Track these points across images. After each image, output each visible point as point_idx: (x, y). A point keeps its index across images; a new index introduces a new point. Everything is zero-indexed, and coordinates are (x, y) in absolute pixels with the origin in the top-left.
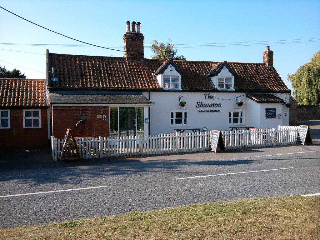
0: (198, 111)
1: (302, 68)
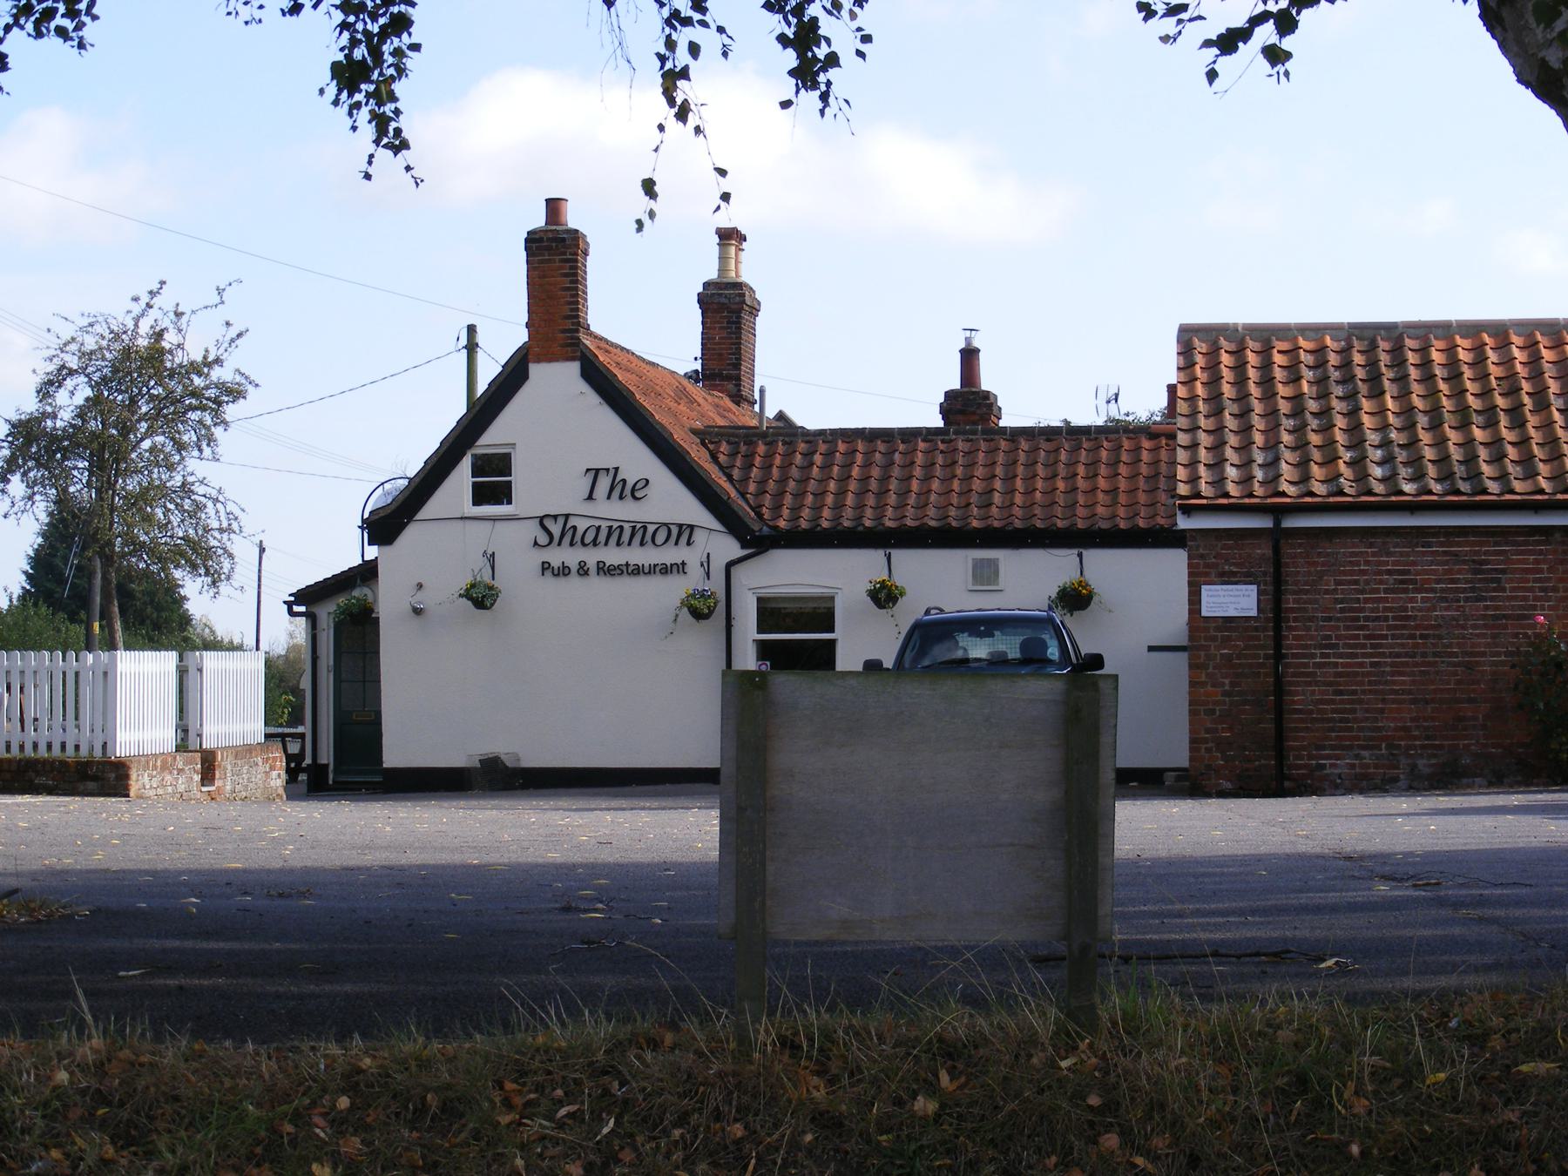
0: (543, 569)
1: (759, 303)
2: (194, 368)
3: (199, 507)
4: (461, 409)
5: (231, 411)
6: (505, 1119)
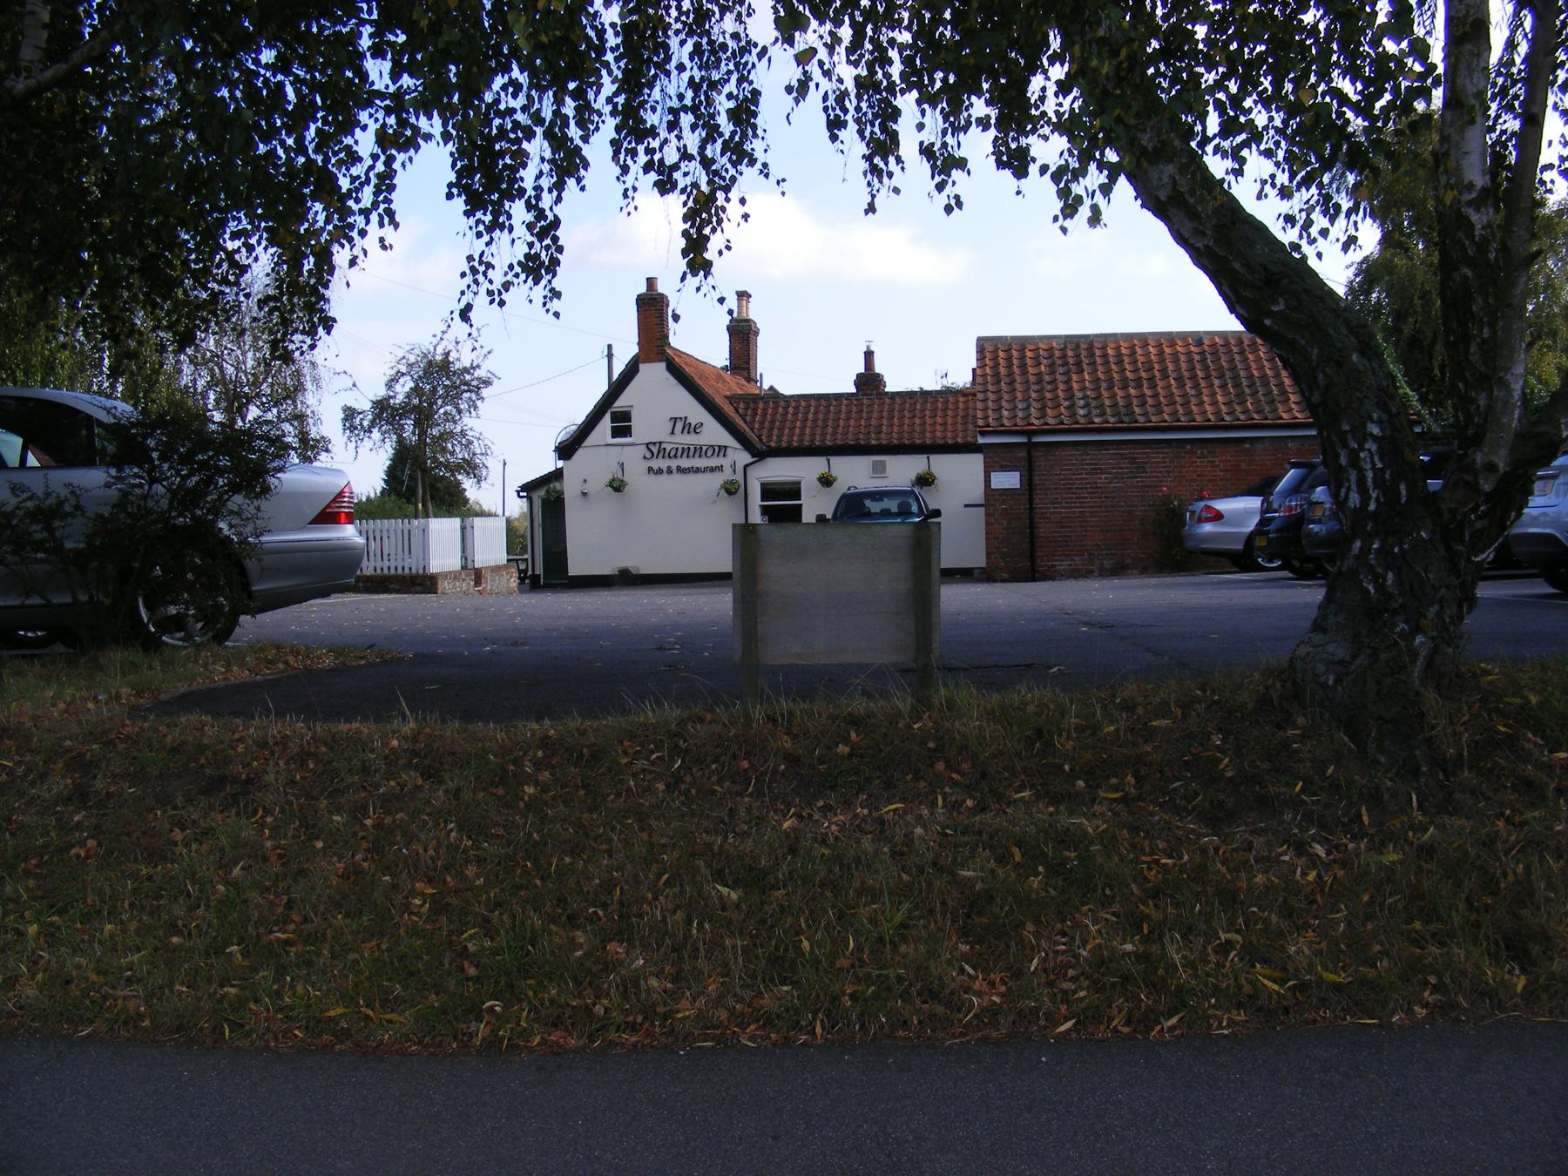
2: (466, 370)
3: (471, 443)
4: (606, 388)
5: (485, 392)
6: (624, 761)
